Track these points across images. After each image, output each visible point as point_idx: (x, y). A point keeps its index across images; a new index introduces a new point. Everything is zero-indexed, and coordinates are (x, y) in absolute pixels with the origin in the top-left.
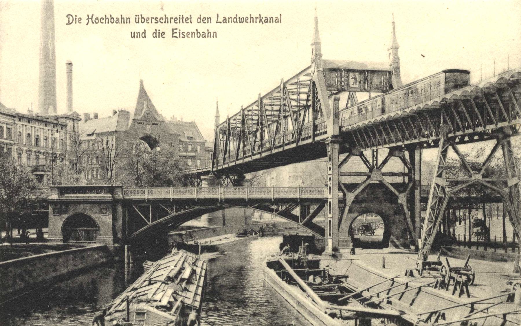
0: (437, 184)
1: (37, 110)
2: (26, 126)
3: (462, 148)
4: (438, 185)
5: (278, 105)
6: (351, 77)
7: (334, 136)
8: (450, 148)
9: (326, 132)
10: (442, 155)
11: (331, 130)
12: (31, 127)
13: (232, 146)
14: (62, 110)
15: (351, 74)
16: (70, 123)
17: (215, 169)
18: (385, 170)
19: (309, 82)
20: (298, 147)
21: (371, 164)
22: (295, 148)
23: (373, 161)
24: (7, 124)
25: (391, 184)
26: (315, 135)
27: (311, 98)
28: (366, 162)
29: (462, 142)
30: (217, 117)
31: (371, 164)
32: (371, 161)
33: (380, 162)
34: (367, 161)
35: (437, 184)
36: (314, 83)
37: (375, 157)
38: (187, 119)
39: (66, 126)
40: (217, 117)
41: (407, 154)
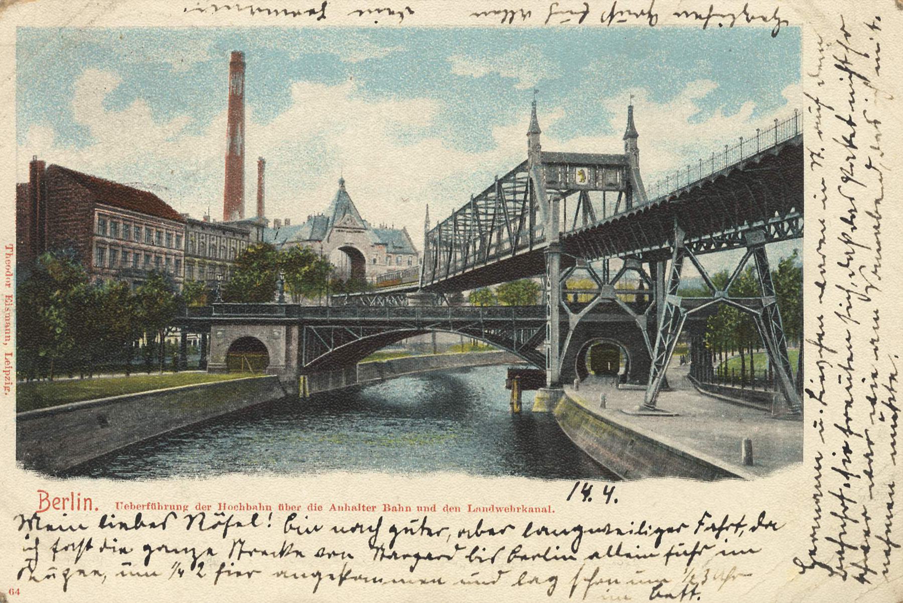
0: (669, 303)
1: (217, 216)
2: (220, 237)
3: (702, 259)
4: (671, 305)
5: (493, 208)
6: (577, 173)
7: (553, 245)
8: (687, 260)
9: (544, 241)
10: (677, 267)
11: (550, 239)
12: (195, 232)
13: (443, 258)
14: (250, 212)
15: (578, 169)
16: (254, 230)
17: (424, 286)
18: (616, 286)
19: (525, 180)
20: (515, 258)
21: (602, 279)
22: (511, 259)
23: (604, 276)
24: (135, 222)
25: (626, 303)
26: (532, 243)
27: (528, 198)
28: (594, 276)
29: (698, 252)
30: (427, 222)
31: (602, 279)
32: (601, 276)
33: (612, 276)
34: (596, 275)
35: (669, 303)
36: (531, 181)
37: (606, 270)
38: (399, 227)
39: (248, 234)
40: (427, 222)
41: (646, 267)
